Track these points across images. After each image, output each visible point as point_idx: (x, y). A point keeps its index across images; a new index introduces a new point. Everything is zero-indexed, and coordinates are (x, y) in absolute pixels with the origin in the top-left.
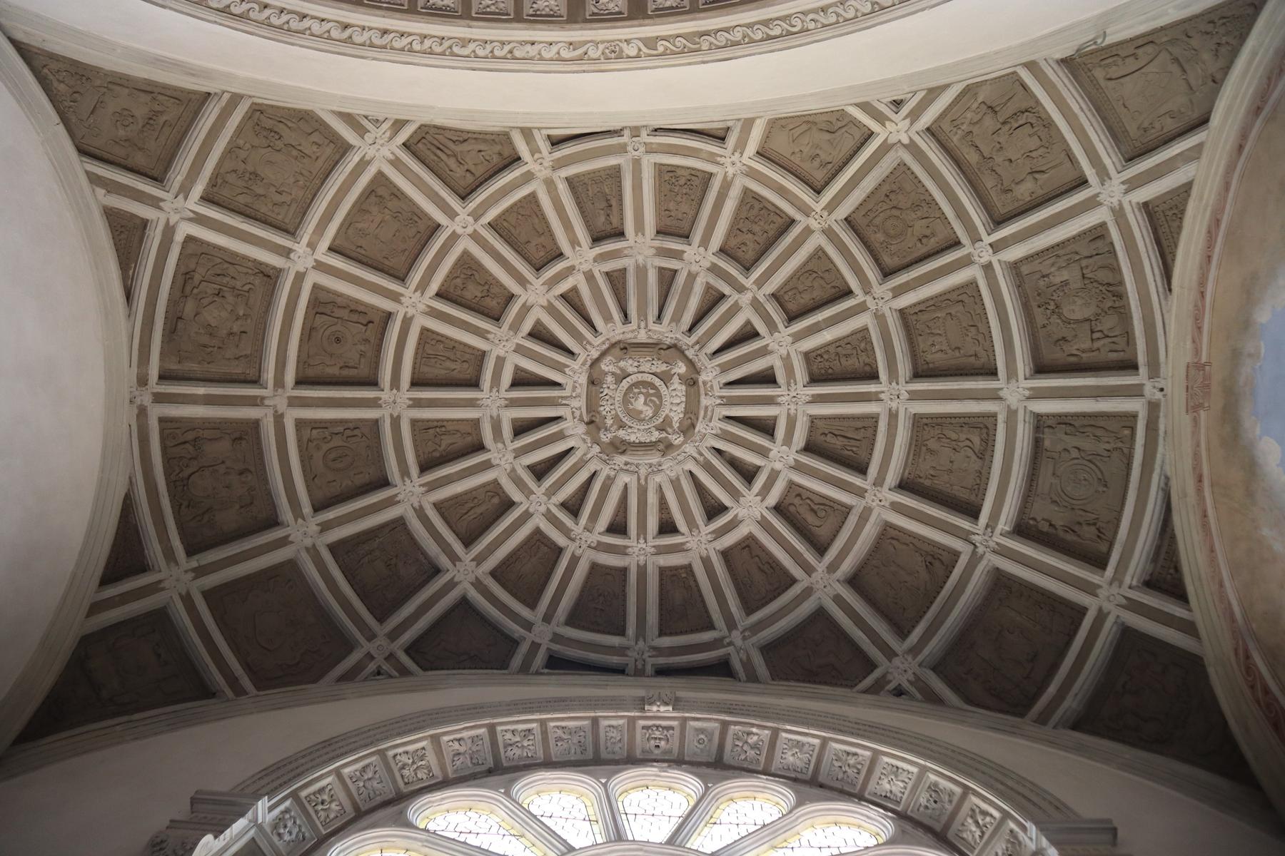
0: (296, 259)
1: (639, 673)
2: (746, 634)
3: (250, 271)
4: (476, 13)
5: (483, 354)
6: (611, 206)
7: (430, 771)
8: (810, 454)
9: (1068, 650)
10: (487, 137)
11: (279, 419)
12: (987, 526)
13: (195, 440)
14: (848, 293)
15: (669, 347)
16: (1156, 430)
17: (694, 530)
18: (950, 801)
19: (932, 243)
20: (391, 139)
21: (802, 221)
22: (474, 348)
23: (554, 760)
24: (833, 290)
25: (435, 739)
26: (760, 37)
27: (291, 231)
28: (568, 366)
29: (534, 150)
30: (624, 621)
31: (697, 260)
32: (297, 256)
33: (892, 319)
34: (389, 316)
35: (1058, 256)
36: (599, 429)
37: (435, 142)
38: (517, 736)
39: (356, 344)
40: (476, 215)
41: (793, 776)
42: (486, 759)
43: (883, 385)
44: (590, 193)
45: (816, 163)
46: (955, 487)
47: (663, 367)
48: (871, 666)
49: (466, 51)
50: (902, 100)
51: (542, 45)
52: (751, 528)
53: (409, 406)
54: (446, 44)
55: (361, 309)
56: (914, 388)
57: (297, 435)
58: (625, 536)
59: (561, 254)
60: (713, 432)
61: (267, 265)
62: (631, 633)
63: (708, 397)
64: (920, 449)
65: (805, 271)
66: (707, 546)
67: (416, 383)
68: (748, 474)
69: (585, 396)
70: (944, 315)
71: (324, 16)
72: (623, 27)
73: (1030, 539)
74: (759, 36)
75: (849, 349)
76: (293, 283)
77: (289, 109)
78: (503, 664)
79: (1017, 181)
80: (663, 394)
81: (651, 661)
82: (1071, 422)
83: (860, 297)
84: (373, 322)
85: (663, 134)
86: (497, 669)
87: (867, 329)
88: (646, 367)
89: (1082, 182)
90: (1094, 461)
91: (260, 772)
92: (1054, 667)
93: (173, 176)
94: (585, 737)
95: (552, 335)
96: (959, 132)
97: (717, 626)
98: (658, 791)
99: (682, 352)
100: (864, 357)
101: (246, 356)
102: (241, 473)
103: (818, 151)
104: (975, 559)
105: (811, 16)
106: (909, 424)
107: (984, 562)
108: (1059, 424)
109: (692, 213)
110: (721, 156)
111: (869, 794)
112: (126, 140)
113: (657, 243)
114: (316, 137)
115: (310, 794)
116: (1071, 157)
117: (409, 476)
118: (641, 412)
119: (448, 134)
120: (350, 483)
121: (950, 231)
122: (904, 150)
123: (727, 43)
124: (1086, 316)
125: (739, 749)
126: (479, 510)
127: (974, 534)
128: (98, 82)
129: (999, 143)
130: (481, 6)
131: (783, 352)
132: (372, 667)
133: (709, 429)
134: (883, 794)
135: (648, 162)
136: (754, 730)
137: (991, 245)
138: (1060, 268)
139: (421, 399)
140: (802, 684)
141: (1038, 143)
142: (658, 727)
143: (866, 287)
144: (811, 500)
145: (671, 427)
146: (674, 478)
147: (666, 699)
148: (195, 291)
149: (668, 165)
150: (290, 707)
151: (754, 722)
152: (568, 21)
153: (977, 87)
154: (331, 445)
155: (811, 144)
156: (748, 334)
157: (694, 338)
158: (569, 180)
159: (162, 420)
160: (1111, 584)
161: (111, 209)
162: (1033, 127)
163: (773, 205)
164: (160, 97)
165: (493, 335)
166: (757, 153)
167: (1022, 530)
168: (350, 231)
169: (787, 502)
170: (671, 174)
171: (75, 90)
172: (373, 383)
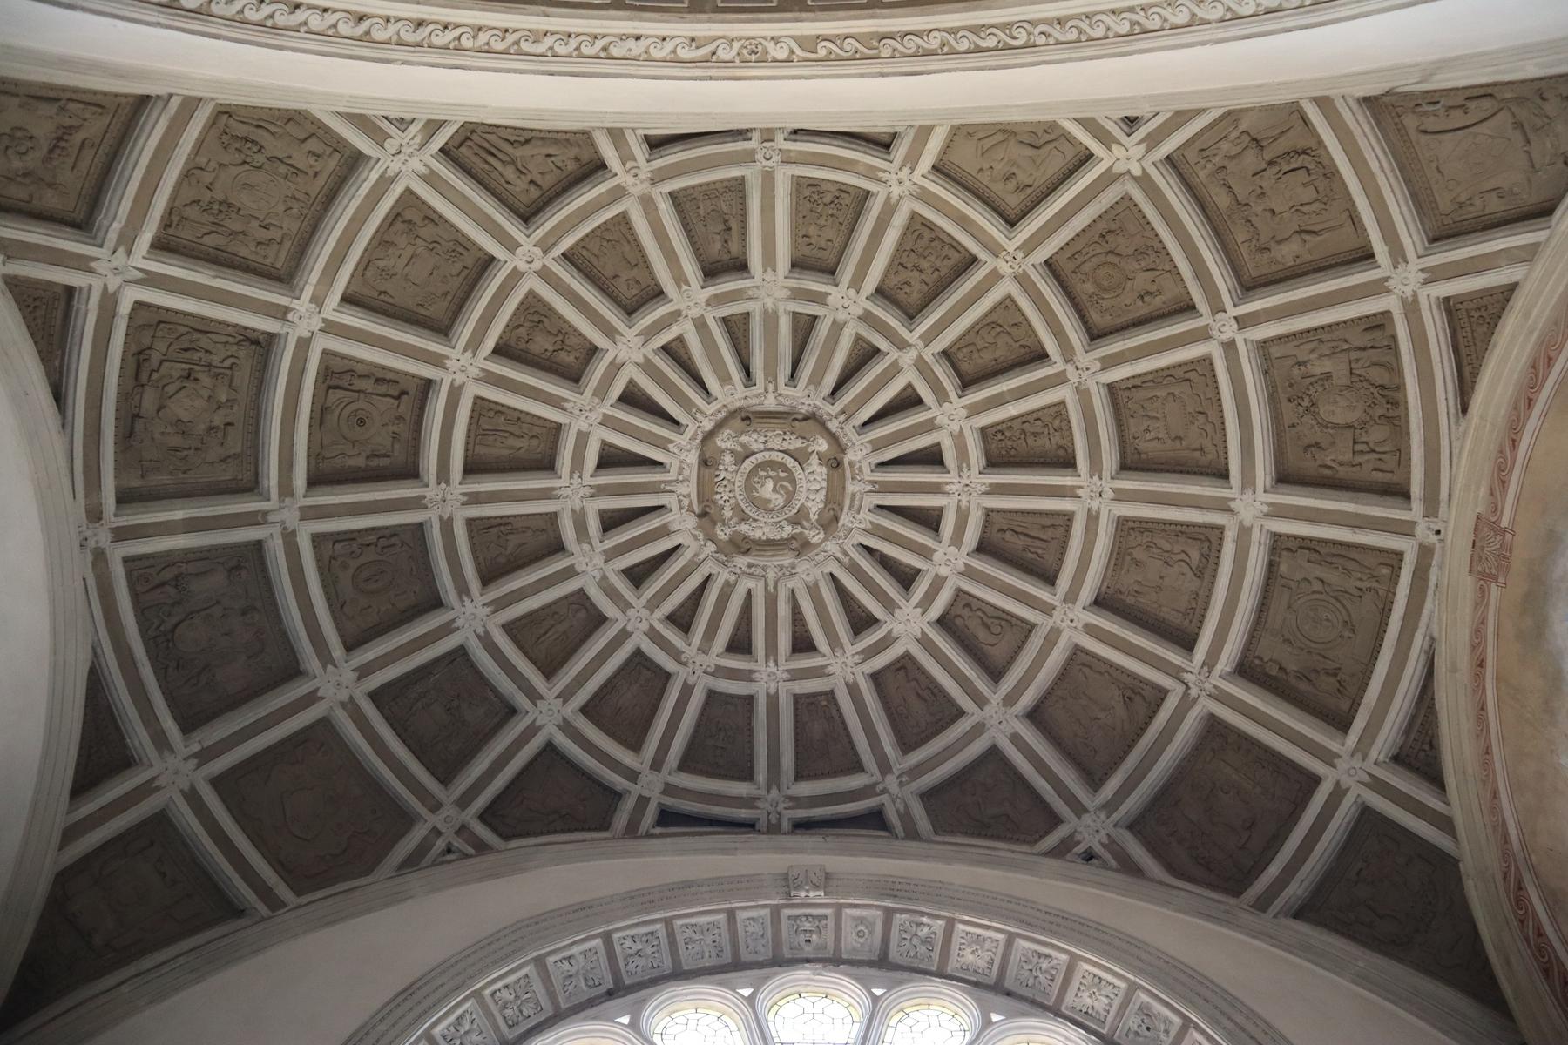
0: (296, 320)
1: (773, 829)
3: (231, 340)
5: (558, 428)
7: (538, 1003)
8: (984, 557)
10: (559, 136)
12: (1204, 664)
13: (177, 578)
14: (1041, 356)
15: (806, 418)
16: (1426, 580)
18: (1167, 1032)
19: (1157, 302)
20: (422, 146)
21: (989, 262)
23: (686, 968)
24: (1023, 351)
27: (285, 278)
28: (672, 442)
29: (626, 157)
32: (297, 315)
34: (428, 385)
36: (714, 523)
40: (546, 246)
42: (603, 977)
44: (701, 212)
45: (1012, 185)
47: (799, 444)
48: (1055, 820)
49: (540, 48)
50: (1137, 118)
54: (511, 38)
55: (390, 376)
57: (315, 553)
59: (661, 293)
60: (862, 526)
62: (761, 779)
64: (1123, 559)
65: (988, 323)
67: (472, 468)
68: (906, 578)
69: (695, 481)
70: (1164, 394)
72: (770, 21)
73: (1253, 682)
74: (965, 45)
75: (1038, 427)
78: (602, 823)
80: (797, 477)
82: (1317, 548)
83: (1058, 364)
84: (407, 393)
85: (805, 138)
86: (595, 829)
88: (776, 443)
89: (1366, 256)
90: (1341, 598)
92: (1278, 839)
93: (106, 223)
94: (720, 935)
96: (1209, 166)
97: (866, 766)
98: (813, 1000)
100: (1057, 438)
102: (244, 613)
103: (1014, 170)
104: (1186, 703)
105: (1042, 28)
109: (839, 242)
110: (884, 171)
111: (1067, 1008)
112: (25, 175)
113: (793, 283)
114: (313, 145)
117: (468, 594)
118: (769, 501)
120: (390, 607)
121: (1183, 290)
122: (1135, 185)
123: (917, 50)
125: (907, 943)
126: (561, 628)
127: (1187, 672)
129: (1261, 187)
131: (955, 427)
132: (440, 844)
133: (858, 522)
134: (1084, 1010)
136: (925, 920)
138: (1321, 356)
139: (478, 493)
141: (1314, 195)
142: (806, 916)
143: (1068, 355)
144: (984, 612)
145: (808, 519)
147: (815, 880)
148: (155, 376)
154: (362, 560)
155: (1006, 160)
156: (908, 401)
157: (839, 406)
158: (673, 196)
160: (1352, 755)
162: (1309, 174)
164: (71, 106)
165: (571, 404)
166: (933, 167)
167: (1246, 670)
168: (369, 274)
169: (952, 613)
170: (814, 189)
172: (411, 473)
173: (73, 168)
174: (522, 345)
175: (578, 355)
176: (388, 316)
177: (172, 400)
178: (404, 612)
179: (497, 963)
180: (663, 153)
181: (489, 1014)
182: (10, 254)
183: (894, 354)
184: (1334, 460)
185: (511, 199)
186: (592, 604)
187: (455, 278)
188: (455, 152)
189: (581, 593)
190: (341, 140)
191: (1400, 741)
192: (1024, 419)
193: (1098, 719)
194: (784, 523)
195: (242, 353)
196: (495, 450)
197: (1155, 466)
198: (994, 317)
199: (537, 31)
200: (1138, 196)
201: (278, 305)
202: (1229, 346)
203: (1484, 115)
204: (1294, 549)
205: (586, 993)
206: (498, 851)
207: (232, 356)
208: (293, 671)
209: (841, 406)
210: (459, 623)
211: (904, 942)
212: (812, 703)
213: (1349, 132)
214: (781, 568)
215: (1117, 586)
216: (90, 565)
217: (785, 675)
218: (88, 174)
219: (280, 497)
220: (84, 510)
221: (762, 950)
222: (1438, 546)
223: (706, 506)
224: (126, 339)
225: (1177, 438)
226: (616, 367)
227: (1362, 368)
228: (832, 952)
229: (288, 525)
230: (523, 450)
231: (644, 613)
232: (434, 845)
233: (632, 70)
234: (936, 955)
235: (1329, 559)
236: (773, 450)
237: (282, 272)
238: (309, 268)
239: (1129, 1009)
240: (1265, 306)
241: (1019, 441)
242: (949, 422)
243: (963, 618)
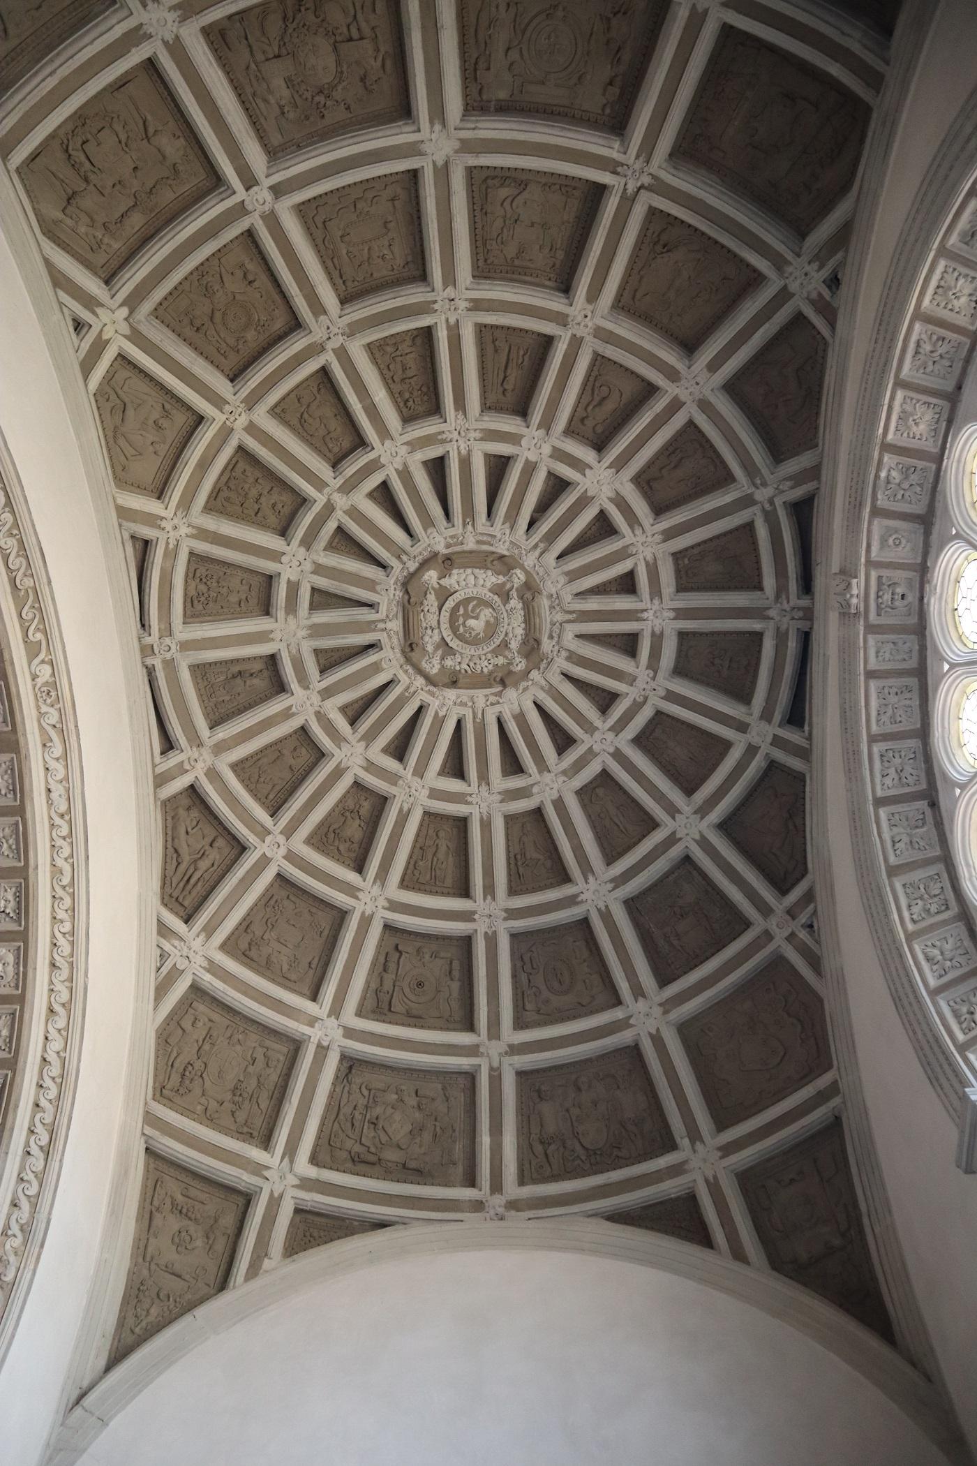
0: (328, 1039)
1: (808, 614)
2: (759, 482)
3: (346, 1089)
4: (20, 861)
5: (428, 814)
6: (240, 672)
7: (931, 877)
8: (530, 410)
9: (781, 49)
11: (514, 1050)
12: (615, 173)
13: (541, 1143)
14: (324, 372)
15: (407, 592)
17: (630, 552)
20: (181, 939)
21: (240, 436)
22: (421, 825)
23: (919, 726)
24: (323, 391)
25: (893, 871)
26: (9, 515)
27: (296, 1046)
28: (437, 713)
29: (181, 770)
30: (744, 633)
31: (298, 563)
33: (352, 315)
34: (388, 928)
35: (254, 94)
36: (510, 673)
37: (182, 885)
39: (424, 963)
40: (263, 833)
41: (944, 424)
42: (917, 810)
43: (438, 321)
44: (227, 698)
45: (165, 423)
48: (799, 319)
50: (74, 320)
51: (50, 779)
54: (60, 892)
55: (382, 959)
56: (440, 280)
58: (640, 636)
60: (508, 532)
61: (338, 1070)
63: (465, 542)
66: (649, 534)
67: (464, 891)
70: (343, 245)
71: (41, 1038)
77: (157, 1057)
78: (799, 779)
79: (161, 158)
80: (463, 596)
81: (794, 601)
82: (473, 61)
85: (146, 617)
86: (804, 786)
87: (369, 345)
88: (432, 619)
89: (151, 65)
90: (523, 26)
91: (934, 1087)
93: (243, 1184)
95: (397, 736)
96: (106, 240)
98: (960, 597)
99: (412, 576)
101: (444, 1089)
102: (579, 1089)
103: (151, 422)
104: (657, 187)
106: (486, 284)
107: (664, 175)
108: (476, 79)
110: (168, 543)
112: (208, 1238)
113: (281, 614)
114: (187, 1024)
115: (962, 1029)
116: (120, 84)
118: (487, 622)
119: (170, 872)
120: (586, 964)
122: (135, 315)
124: (331, 49)
125: (907, 494)
127: (625, 189)
128: (145, 1272)
129: (114, 185)
130: (11, 856)
131: (403, 450)
132: (803, 935)
135: (183, 633)
136: (883, 474)
137: (247, 189)
138: (269, 90)
139: (484, 887)
140: (823, 406)
143: (319, 348)
144: (588, 405)
145: (504, 584)
146: (567, 578)
147: (843, 586)
148: (373, 1150)
149: (185, 607)
150: (852, 1035)
151: (872, 476)
152: (17, 751)
153: (44, 221)
154: (543, 987)
155: (144, 433)
156: (384, 496)
159: (522, 1182)
161: (286, 1249)
162: (87, 141)
163: (222, 474)
164: (156, 1203)
166: (159, 498)
167: (618, 125)
168: (293, 977)
170: (195, 602)
171: (156, 1297)
172: (466, 942)
174: (356, 846)
175: (363, 798)
176: (329, 962)
177: (392, 1137)
178: (591, 951)
179: (887, 915)
180: (175, 739)
181: (932, 928)
182: (264, 1254)
185: (227, 862)
186: (591, 782)
187: (297, 905)
188: (189, 910)
189: (580, 793)
190: (181, 1002)
192: (390, 381)
193: (690, 277)
195: (358, 1081)
197: (418, 244)
198: (295, 422)
199: (52, 872)
200: (147, 306)
201: (316, 1053)
204: (479, 87)
205: (929, 829)
207: (360, 1088)
208: (634, 1051)
212: (686, 572)
213: (27, 115)
214: (552, 607)
215: (548, 270)
216: (519, 1213)
217: (656, 601)
219: (478, 1056)
220: (473, 1214)
221: (908, 644)
223: (495, 680)
224: (340, 1171)
225: (386, 227)
227: (270, 45)
228: (915, 573)
230: (449, 844)
231: (597, 735)
233: (78, 792)
234: (920, 464)
235: (483, 45)
236: (439, 621)
237: (292, 1048)
238: (284, 1028)
239: (967, 256)
240: (227, 161)
241: (413, 383)
243: (596, 425)
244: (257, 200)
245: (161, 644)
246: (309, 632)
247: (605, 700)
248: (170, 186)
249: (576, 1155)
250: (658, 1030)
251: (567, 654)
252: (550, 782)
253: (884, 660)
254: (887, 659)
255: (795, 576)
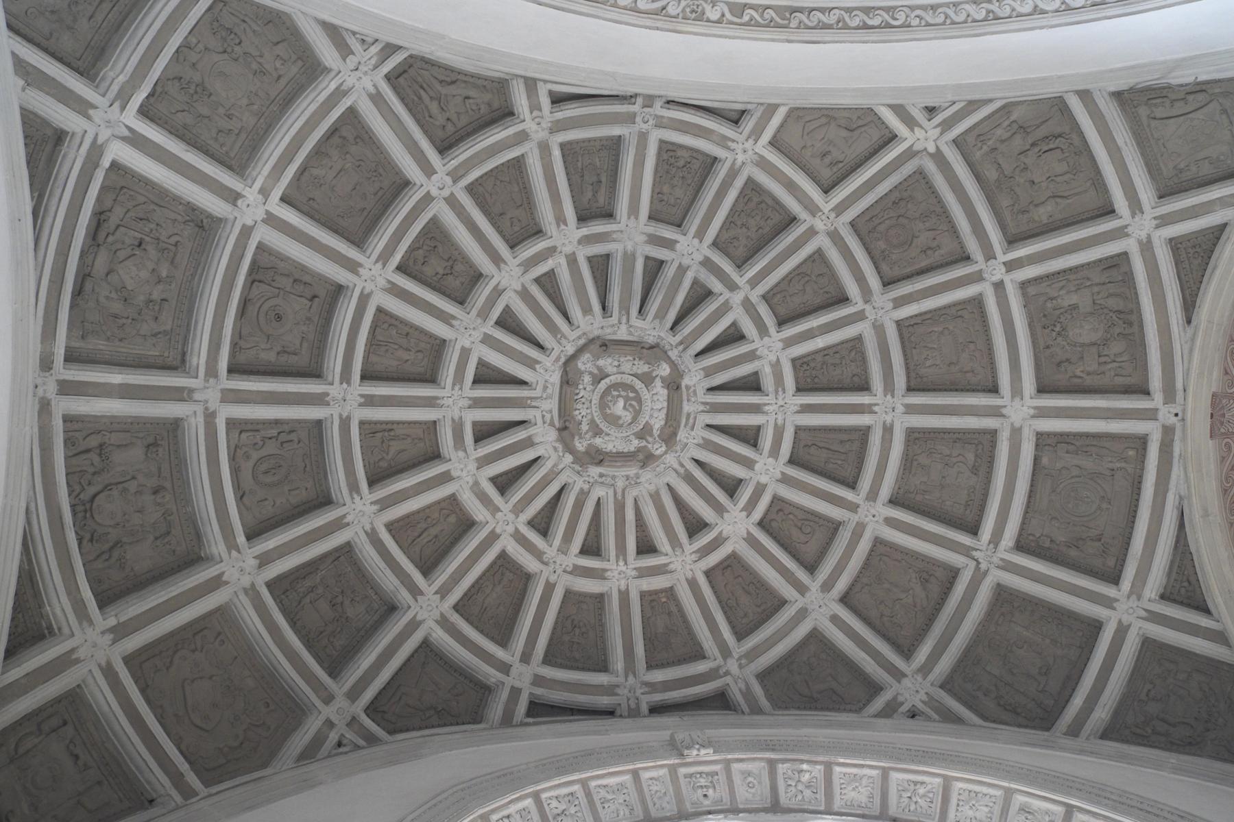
0: (244, 207)
1: (634, 713)
2: (743, 661)
3: (179, 218)
11: (210, 417)
12: (990, 543)
13: (101, 446)
14: (843, 300)
15: (652, 347)
19: (936, 257)
20: (376, 67)
29: (535, 106)
36: (573, 436)
38: (563, 802)
39: (298, 324)
40: (456, 176)
45: (827, 160)
46: (948, 503)
48: (875, 689)
52: (737, 546)
53: (361, 405)
55: (307, 278)
60: (695, 441)
63: (691, 403)
69: (557, 398)
74: (856, 22)
76: (237, 240)
78: (475, 716)
85: (676, 107)
88: (626, 367)
89: (1108, 211)
97: (709, 652)
101: (165, 333)
102: (155, 492)
105: (918, 12)
110: (733, 141)
114: (280, 50)
117: (358, 492)
118: (619, 418)
124: (1093, 340)
126: (434, 531)
127: (976, 550)
129: (1024, 164)
132: (333, 737)
133: (691, 437)
136: (805, 767)
138: (1069, 292)
139: (372, 396)
142: (701, 773)
145: (651, 435)
148: (110, 239)
151: (802, 757)
154: (264, 452)
155: (826, 139)
156: (734, 336)
159: (67, 419)
160: (1128, 597)
167: (1021, 546)
170: (672, 154)
172: (314, 372)
173: (90, 18)
180: (562, 108)
183: (727, 294)
184: (1082, 372)
191: (1164, 582)
192: (826, 352)
194: (632, 437)
196: (386, 362)
197: (936, 387)
202: (999, 286)
203: (1203, 104)
206: (387, 743)
209: (681, 338)
210: (349, 519)
211: (790, 789)
212: (654, 600)
214: (628, 478)
218: (100, 27)
221: (668, 807)
222: (1178, 425)
226: (498, 292)
229: (209, 405)
231: (511, 517)
232: (328, 737)
234: (821, 796)
235: (1085, 449)
240: (1028, 253)
242: (769, 353)
244: (995, 269)
245: (651, 115)
246: (629, 252)
247: (542, 525)
248: (1013, 205)
249: (86, 487)
250: (227, 583)
251: (585, 490)
252: (468, 468)
253: (649, 785)
254: (651, 788)
255: (666, 698)
